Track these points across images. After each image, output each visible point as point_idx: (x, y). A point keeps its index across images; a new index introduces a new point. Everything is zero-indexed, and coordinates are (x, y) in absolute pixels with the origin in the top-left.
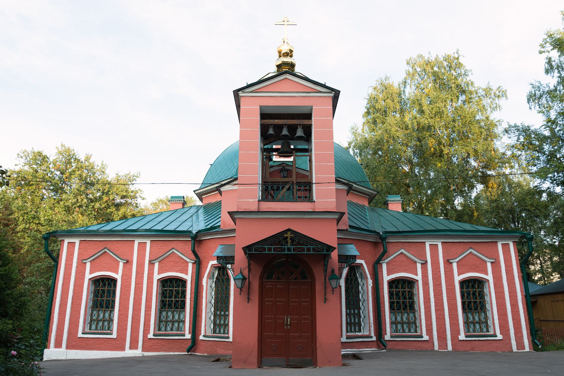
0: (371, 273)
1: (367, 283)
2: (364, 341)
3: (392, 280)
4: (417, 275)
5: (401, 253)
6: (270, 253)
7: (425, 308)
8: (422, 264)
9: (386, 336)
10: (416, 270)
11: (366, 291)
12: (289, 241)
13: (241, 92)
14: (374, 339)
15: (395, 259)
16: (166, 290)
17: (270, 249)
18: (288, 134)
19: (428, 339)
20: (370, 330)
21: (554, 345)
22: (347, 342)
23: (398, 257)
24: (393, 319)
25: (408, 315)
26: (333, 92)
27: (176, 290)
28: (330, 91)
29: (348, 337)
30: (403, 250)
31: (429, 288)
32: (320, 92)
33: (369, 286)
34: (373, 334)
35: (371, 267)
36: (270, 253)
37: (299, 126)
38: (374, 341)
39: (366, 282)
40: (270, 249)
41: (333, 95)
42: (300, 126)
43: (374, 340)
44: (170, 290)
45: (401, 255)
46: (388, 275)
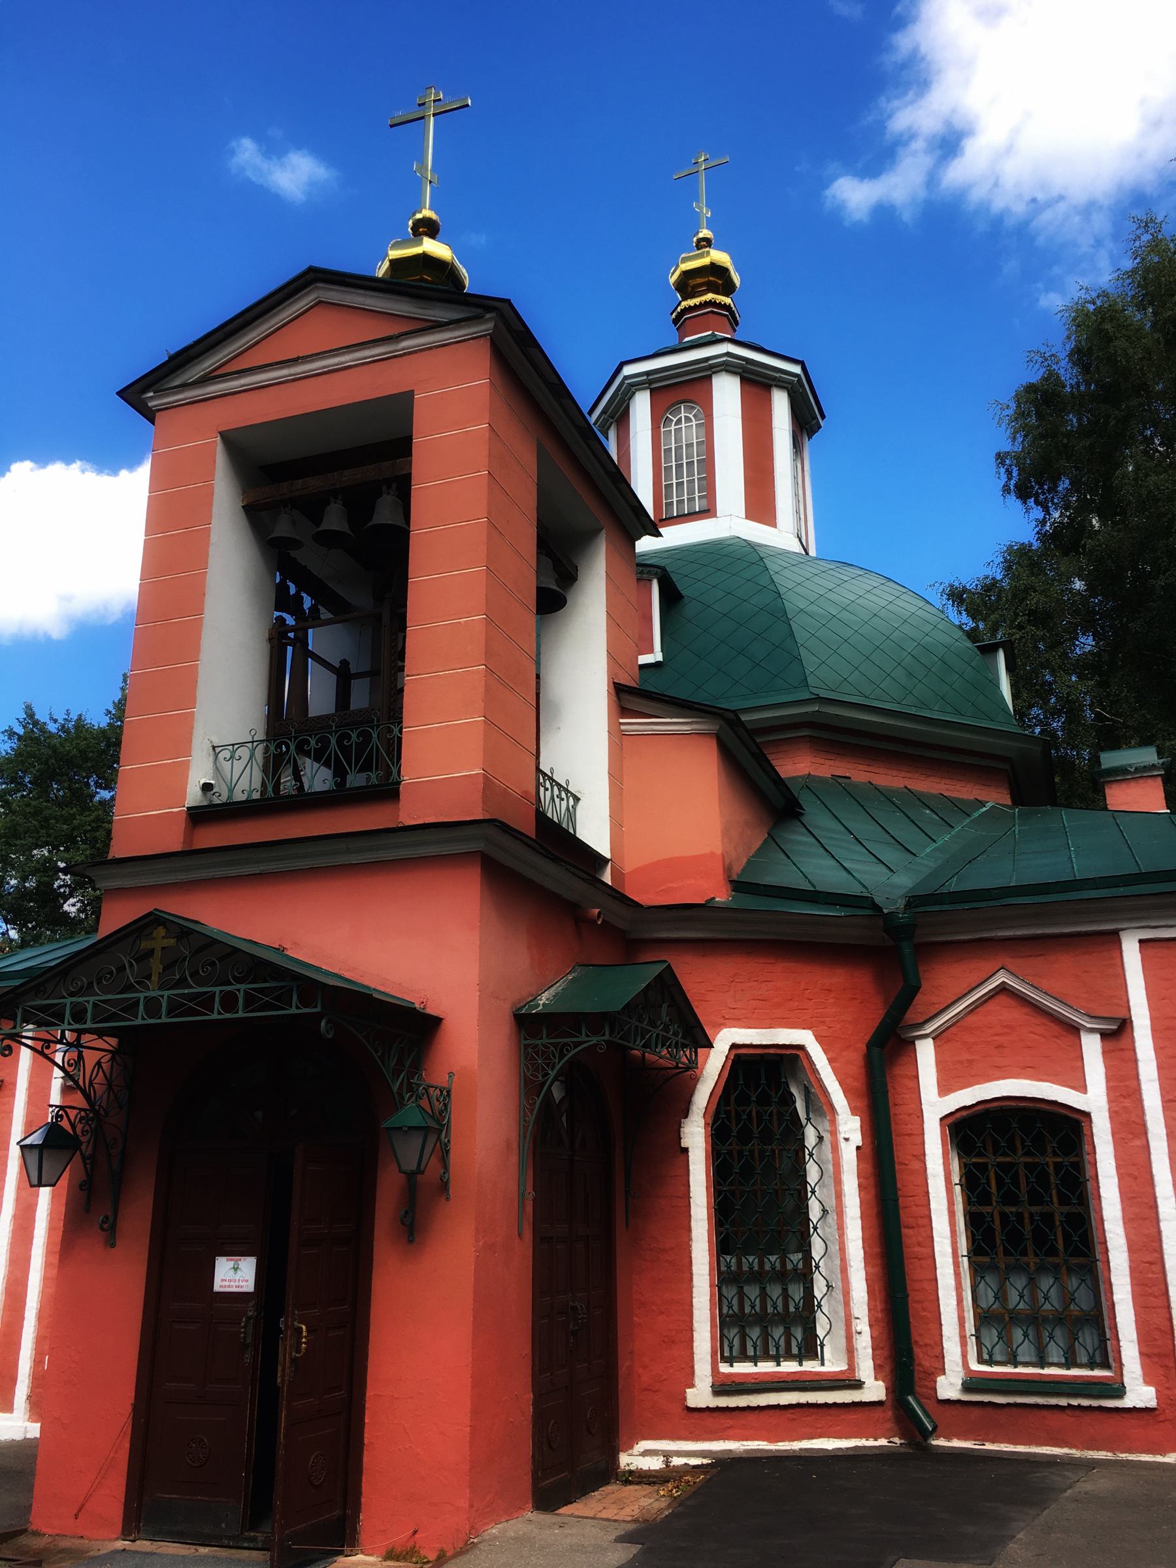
0: (859, 1084)
1: (834, 1133)
2: (808, 1405)
3: (964, 1113)
4: (1082, 1088)
5: (1003, 989)
6: (228, 1016)
7: (1132, 1249)
8: (1105, 1035)
9: (941, 1380)
10: (1079, 1064)
11: (831, 1167)
12: (156, 966)
13: (151, 394)
14: (874, 1390)
15: (972, 1018)
16: (982, 1168)
17: (229, 1002)
18: (371, 524)
19: (1153, 1404)
20: (851, 1351)
21: (473, 1528)
22: (718, 1409)
23: (990, 1006)
24: (988, 1299)
25: (1032, 1283)
26: (488, 316)
27: (1029, 1167)
28: (479, 311)
29: (722, 1387)
30: (1008, 975)
31: (1147, 1148)
32: (437, 326)
33: (843, 1144)
34: (866, 1369)
35: (855, 1057)
36: (228, 1016)
37: (384, 488)
38: (879, 1403)
39: (827, 1125)
40: (229, 1002)
41: (491, 325)
42: (389, 488)
43: (875, 1398)
44: (1005, 1167)
45: (1003, 999)
46: (945, 1088)
